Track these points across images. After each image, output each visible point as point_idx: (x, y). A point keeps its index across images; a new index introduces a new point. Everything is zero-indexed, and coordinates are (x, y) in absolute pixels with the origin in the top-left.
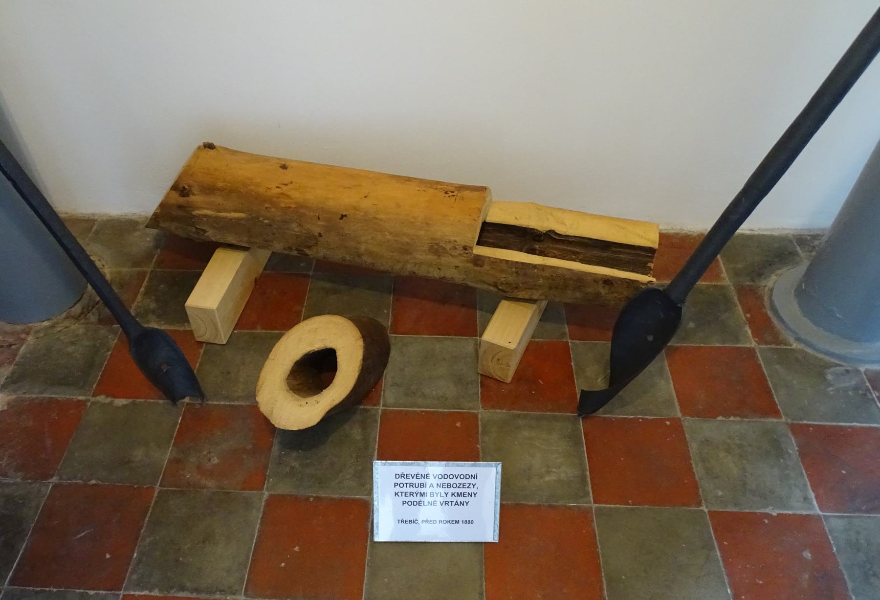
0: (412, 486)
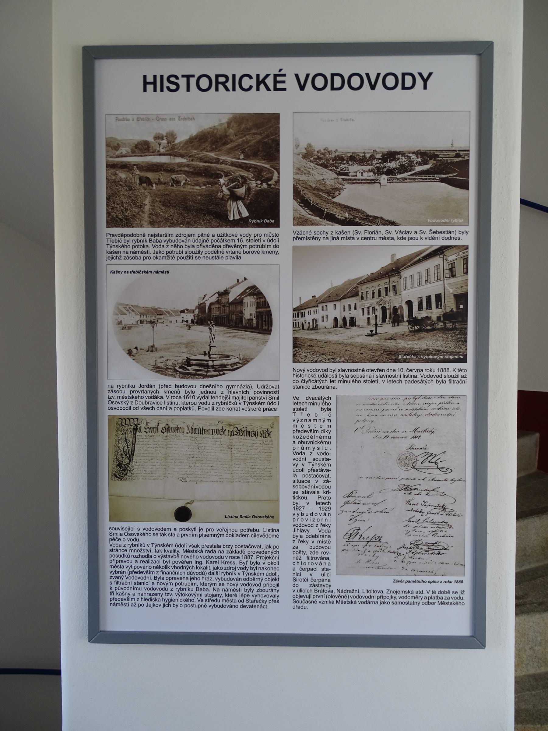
0: (223, 84)
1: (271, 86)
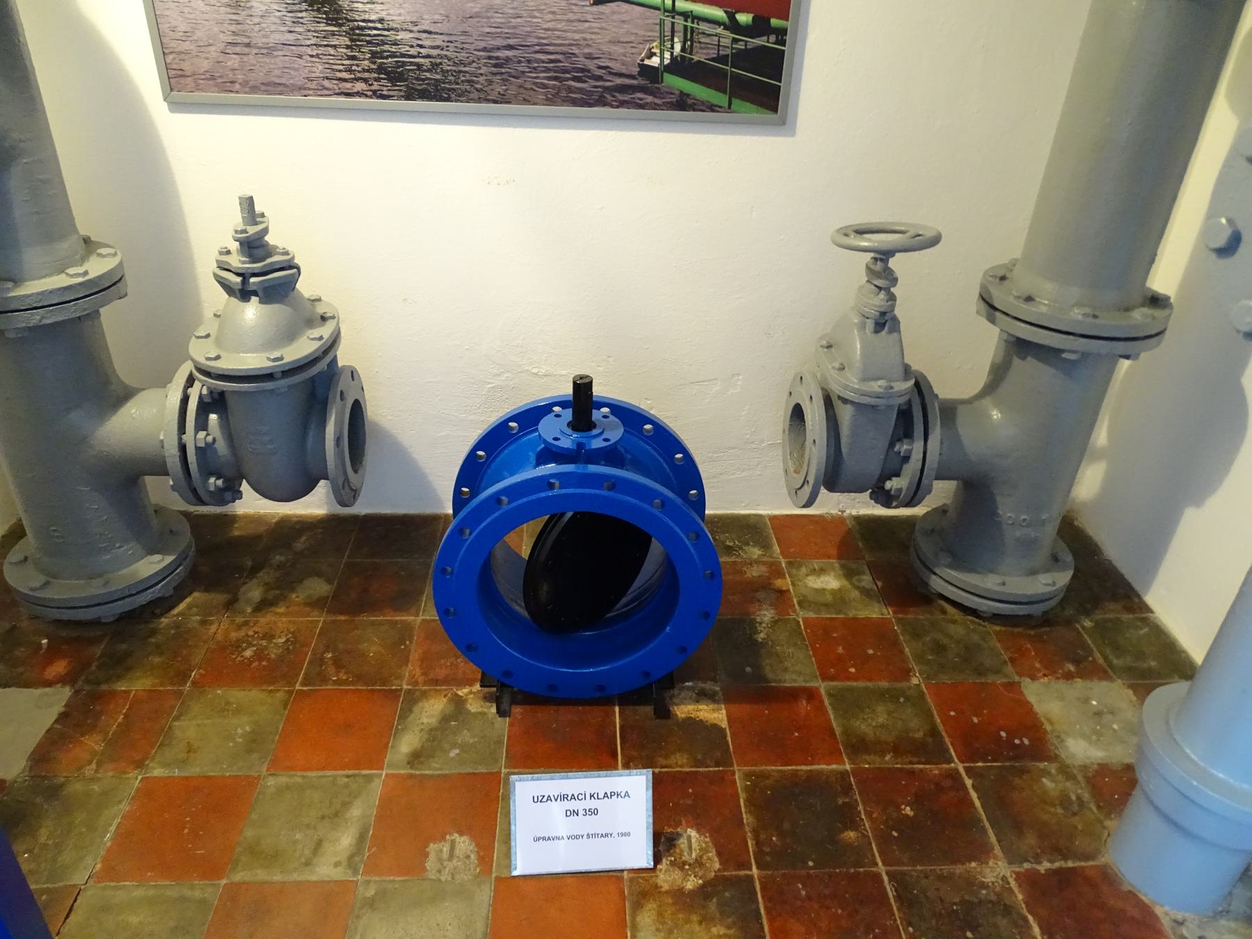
1: (596, 797)
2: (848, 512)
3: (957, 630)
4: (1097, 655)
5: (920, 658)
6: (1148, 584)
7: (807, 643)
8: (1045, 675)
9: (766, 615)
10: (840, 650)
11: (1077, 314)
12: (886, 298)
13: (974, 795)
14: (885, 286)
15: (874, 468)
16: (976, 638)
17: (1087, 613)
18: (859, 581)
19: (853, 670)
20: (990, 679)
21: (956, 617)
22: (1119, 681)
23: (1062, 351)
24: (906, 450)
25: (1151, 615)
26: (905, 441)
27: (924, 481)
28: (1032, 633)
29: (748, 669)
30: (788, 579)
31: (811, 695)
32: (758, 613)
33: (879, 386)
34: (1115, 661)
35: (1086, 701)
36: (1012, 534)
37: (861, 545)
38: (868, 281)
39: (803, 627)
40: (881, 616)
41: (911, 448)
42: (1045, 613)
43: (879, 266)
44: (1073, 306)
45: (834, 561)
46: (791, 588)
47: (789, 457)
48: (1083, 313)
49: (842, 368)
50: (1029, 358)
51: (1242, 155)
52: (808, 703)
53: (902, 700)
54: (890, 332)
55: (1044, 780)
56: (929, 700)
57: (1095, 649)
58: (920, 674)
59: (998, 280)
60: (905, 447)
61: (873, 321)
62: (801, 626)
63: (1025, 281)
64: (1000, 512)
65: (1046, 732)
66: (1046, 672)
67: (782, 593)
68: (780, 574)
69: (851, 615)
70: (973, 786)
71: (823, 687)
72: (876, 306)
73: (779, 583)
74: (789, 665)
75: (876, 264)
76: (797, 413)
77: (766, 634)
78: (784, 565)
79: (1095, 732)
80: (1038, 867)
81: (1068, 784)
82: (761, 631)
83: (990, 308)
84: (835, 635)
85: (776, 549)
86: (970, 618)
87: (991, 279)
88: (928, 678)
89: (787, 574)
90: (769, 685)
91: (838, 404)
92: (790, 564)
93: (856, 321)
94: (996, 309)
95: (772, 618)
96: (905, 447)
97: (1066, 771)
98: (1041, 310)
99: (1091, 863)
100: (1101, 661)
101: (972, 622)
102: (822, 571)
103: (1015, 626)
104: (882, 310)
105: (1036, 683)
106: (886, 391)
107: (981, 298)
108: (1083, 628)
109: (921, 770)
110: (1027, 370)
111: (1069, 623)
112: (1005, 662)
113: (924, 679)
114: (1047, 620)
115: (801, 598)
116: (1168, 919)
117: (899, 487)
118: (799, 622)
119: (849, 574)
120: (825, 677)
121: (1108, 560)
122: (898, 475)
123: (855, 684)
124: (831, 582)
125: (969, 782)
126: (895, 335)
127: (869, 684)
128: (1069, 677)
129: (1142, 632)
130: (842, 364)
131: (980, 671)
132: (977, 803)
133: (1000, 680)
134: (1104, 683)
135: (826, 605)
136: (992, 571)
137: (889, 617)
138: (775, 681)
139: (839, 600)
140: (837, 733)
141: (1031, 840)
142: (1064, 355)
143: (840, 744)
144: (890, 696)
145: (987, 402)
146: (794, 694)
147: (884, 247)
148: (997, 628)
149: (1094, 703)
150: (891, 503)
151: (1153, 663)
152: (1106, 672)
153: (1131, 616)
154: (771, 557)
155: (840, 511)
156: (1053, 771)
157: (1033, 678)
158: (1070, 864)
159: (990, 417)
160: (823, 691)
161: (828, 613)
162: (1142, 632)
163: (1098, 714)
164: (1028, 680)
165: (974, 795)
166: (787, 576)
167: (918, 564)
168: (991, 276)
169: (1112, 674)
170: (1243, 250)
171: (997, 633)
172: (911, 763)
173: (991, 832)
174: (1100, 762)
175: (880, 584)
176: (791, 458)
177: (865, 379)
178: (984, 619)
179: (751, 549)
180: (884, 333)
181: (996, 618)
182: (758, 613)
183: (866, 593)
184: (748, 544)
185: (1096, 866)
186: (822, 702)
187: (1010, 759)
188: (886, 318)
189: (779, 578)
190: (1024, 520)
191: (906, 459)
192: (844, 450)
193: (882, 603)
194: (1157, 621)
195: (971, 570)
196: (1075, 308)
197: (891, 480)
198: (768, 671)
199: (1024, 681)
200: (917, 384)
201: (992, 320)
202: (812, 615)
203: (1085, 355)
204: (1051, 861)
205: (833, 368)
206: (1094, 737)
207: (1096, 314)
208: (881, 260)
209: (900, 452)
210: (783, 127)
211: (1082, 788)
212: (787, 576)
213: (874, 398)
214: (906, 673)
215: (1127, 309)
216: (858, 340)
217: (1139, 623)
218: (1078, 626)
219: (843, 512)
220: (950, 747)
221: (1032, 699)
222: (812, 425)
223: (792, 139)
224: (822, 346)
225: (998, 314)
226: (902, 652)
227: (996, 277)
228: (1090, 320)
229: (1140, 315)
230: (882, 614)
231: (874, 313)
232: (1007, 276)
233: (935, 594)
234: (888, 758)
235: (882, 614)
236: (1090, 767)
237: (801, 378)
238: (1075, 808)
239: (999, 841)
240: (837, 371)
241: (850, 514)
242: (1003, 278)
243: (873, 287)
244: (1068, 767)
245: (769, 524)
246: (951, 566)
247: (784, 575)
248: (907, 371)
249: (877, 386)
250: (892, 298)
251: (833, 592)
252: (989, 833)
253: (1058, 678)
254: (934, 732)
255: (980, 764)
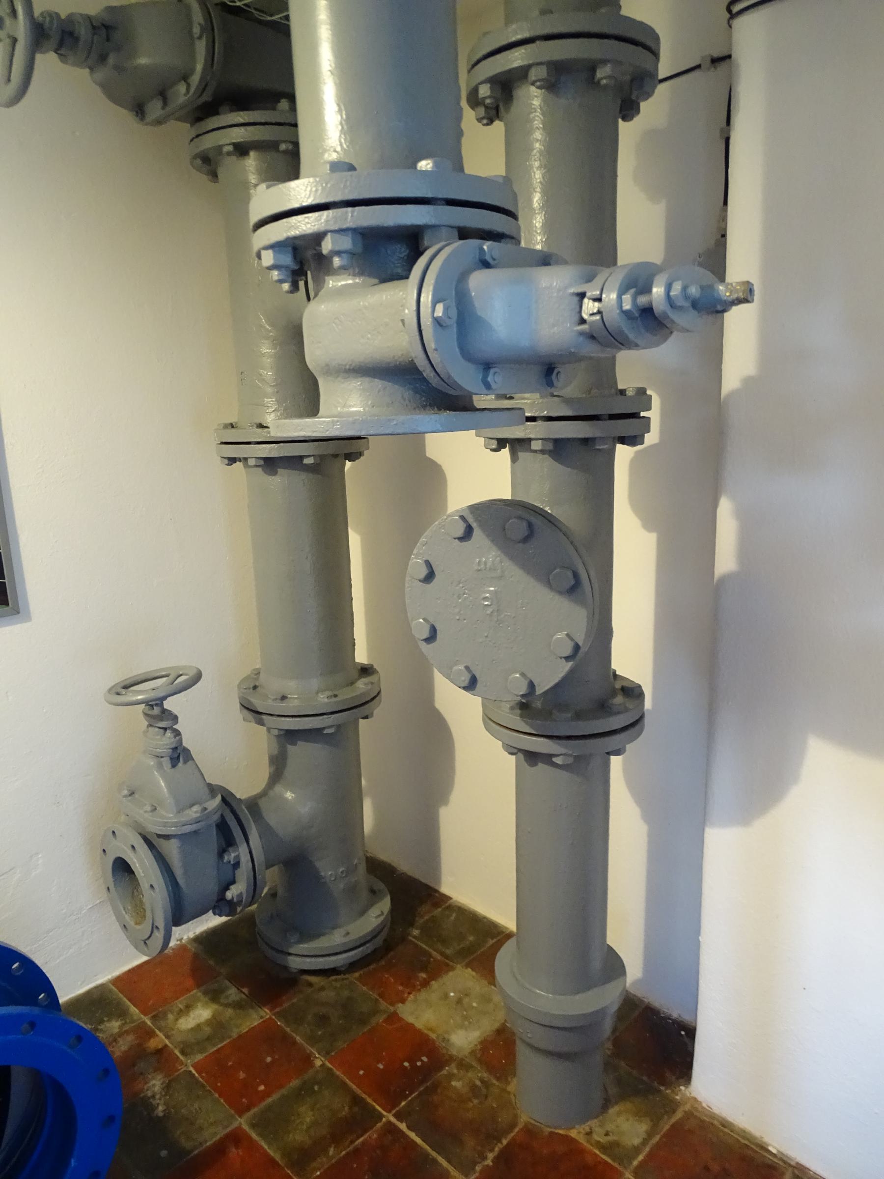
2: (185, 937)
3: (328, 995)
4: (434, 953)
5: (312, 1040)
6: (438, 879)
7: (208, 1088)
8: (409, 993)
9: (155, 1084)
10: (242, 1075)
11: (323, 698)
12: (172, 736)
13: (412, 1135)
14: (169, 726)
15: (211, 887)
16: (346, 993)
17: (412, 924)
18: (227, 997)
19: (262, 1088)
20: (374, 1021)
21: (322, 983)
22: (459, 966)
23: (324, 728)
24: (235, 857)
25: (451, 901)
26: (231, 849)
27: (259, 877)
28: (383, 963)
29: (164, 1153)
30: (161, 1035)
31: (236, 1138)
32: (146, 1087)
33: (196, 812)
34: (448, 952)
35: (446, 996)
36: (338, 888)
37: (211, 962)
38: (150, 725)
39: (197, 1075)
40: (262, 1020)
41: (237, 853)
42: (385, 940)
43: (156, 711)
44: (317, 693)
45: (195, 991)
46: (167, 1042)
47: (124, 913)
48: (326, 696)
49: (154, 809)
50: (299, 743)
51: (561, 658)
52: (237, 1147)
53: (316, 1088)
54: (185, 762)
55: (453, 1083)
56: (338, 1073)
57: (431, 950)
58: (319, 1054)
59: (252, 690)
60: (233, 855)
61: (168, 758)
62: (194, 1075)
63: (273, 684)
64: (322, 874)
65: (433, 1040)
66: (408, 990)
67: (161, 1052)
68: (151, 1034)
69: (235, 1035)
70: (409, 1127)
71: (243, 1122)
72: (167, 745)
73: (153, 1044)
74: (202, 1121)
75: (153, 709)
76: (122, 868)
77: (165, 1104)
78: (149, 1023)
79: (465, 1018)
80: (486, 1163)
81: (470, 1074)
82: (158, 1104)
83: (256, 714)
84: (230, 1063)
85: (134, 1010)
86: (334, 977)
87: (245, 691)
88: (328, 1053)
89: (156, 1030)
90: (192, 1155)
91: (156, 841)
92: (154, 1018)
93: (152, 763)
94: (261, 713)
95: (162, 1084)
96: (233, 855)
97: (462, 1065)
98: (294, 705)
99: (516, 1130)
100: (439, 957)
101: (336, 980)
102: (189, 1008)
103: (369, 964)
104: (173, 746)
105: (407, 1003)
106: (202, 814)
107: (242, 707)
108: (415, 937)
109: (363, 1143)
110: (299, 752)
111: (404, 939)
112: (377, 1000)
113: (324, 1057)
114: (388, 947)
115: (182, 1046)
116: (581, 1135)
117: (239, 892)
118: (190, 1071)
119: (214, 996)
120: (241, 1113)
121: (403, 873)
122: (233, 882)
123: (270, 1100)
124: (202, 1014)
125: (403, 1126)
126: (190, 762)
127: (284, 1091)
128: (425, 984)
129: (452, 918)
130: (153, 805)
131: (363, 1022)
132: (418, 1140)
133: (381, 1019)
134: (451, 974)
135: (208, 1039)
136: (334, 928)
137: (268, 1016)
138: (195, 1148)
139: (217, 1025)
140: (277, 1159)
141: (470, 1142)
142: (325, 732)
143: (286, 1169)
144: (304, 1092)
145: (278, 788)
146: (219, 1150)
147: (153, 695)
148: (357, 975)
149: (452, 994)
150: (236, 909)
151: (471, 938)
152: (448, 965)
153: (440, 910)
154: (134, 1021)
155: (178, 941)
156: (455, 1071)
157: (403, 1001)
158: (505, 1142)
159: (286, 799)
160: (245, 1127)
161: (214, 1045)
162: (452, 918)
163: (459, 1001)
164: (400, 1005)
165: (412, 1135)
166: (158, 1032)
167: (270, 953)
168: (245, 689)
169: (451, 963)
170: (439, 635)
171: (360, 979)
172: (352, 1142)
173: (440, 1160)
174: (480, 1040)
175: (245, 990)
176: (126, 913)
177: (180, 811)
178: (344, 973)
179: (108, 1025)
180: (180, 764)
181: (353, 966)
182: (146, 1087)
183: (238, 1006)
184: (101, 1022)
185: (521, 1130)
186: (249, 1138)
187: (422, 1082)
188: (178, 752)
189: (150, 1038)
190: (342, 872)
191: (237, 865)
192: (181, 881)
193: (257, 1007)
194: (457, 904)
195: (318, 936)
196: (319, 694)
197: (229, 889)
198: (187, 1144)
199: (398, 1007)
200: (224, 799)
201: (261, 723)
202: (199, 1057)
203: (339, 727)
204: (492, 1150)
205: (146, 812)
206: (466, 1023)
207: (335, 693)
208: (157, 705)
209: (230, 862)
210: (17, 616)
211: (479, 1072)
212: (158, 1032)
213: (194, 824)
214: (308, 1060)
215: (352, 683)
216: (160, 779)
217: (447, 912)
218: (410, 938)
219: (181, 940)
220: (374, 1104)
221: (410, 1019)
222: (143, 872)
223: (29, 624)
224: (125, 796)
225: (264, 717)
226: (295, 1043)
227: (249, 688)
228: (334, 700)
229: (362, 685)
230: (262, 1017)
231: (165, 750)
232: (257, 684)
233: (296, 973)
234: (331, 1151)
235: (262, 1017)
236: (476, 1050)
237: (114, 832)
238: (484, 1091)
239: (449, 1162)
240: (151, 814)
241: (188, 938)
242: (255, 687)
243: (157, 729)
244: (462, 1059)
245: (115, 989)
246: (300, 941)
247: (154, 1032)
248: (213, 790)
249: (194, 812)
250: (177, 733)
251: (209, 1022)
252: (439, 1160)
253: (419, 990)
254: (356, 1100)
255: (403, 1103)
